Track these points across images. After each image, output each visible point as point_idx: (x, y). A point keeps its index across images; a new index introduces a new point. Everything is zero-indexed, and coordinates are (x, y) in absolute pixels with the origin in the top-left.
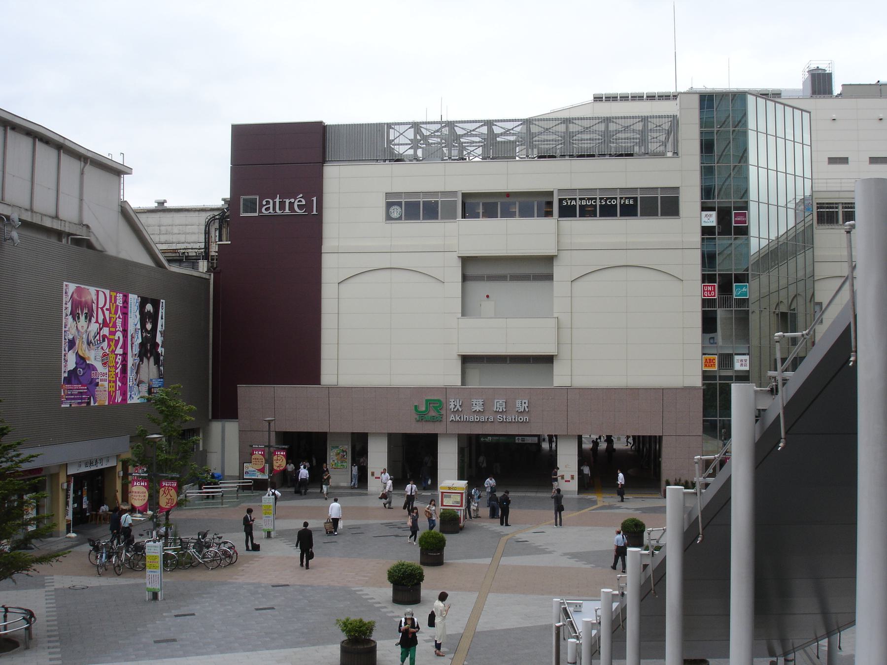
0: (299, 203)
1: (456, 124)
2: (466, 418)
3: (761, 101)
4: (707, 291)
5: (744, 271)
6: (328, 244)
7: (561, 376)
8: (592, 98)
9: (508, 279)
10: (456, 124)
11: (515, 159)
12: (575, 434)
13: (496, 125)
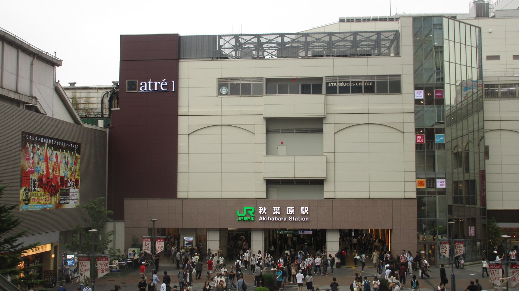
0: (163, 85)
2: (270, 219)
3: (451, 21)
4: (419, 139)
5: (430, 127)
7: (328, 192)
8: (338, 20)
9: (295, 132)
13: (287, 37)
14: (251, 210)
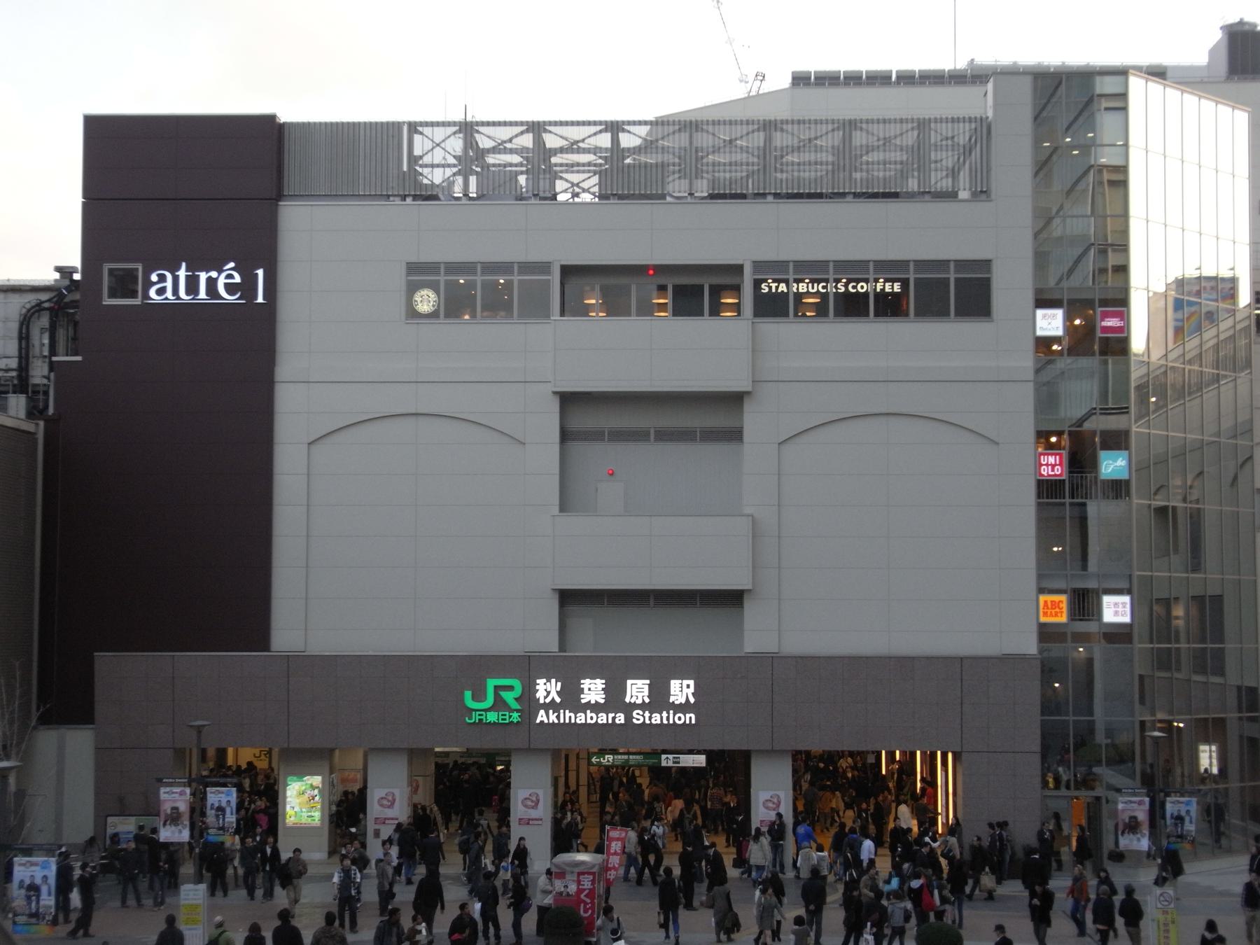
1: (476, 128)
2: (570, 717)
4: (1047, 465)
6: (287, 367)
8: (789, 80)
10: (476, 128)
11: (665, 199)
12: (789, 748)
14: (510, 688)
